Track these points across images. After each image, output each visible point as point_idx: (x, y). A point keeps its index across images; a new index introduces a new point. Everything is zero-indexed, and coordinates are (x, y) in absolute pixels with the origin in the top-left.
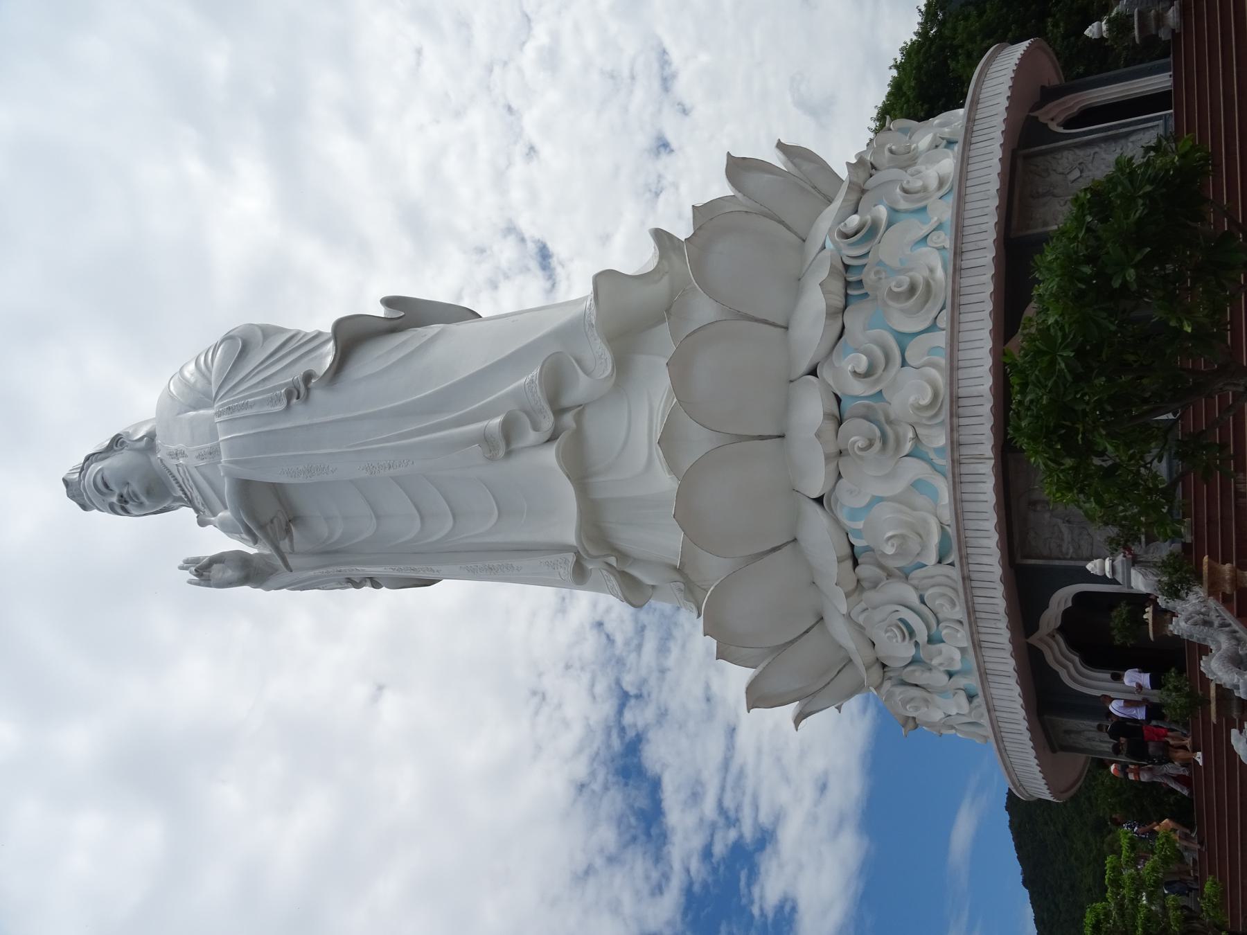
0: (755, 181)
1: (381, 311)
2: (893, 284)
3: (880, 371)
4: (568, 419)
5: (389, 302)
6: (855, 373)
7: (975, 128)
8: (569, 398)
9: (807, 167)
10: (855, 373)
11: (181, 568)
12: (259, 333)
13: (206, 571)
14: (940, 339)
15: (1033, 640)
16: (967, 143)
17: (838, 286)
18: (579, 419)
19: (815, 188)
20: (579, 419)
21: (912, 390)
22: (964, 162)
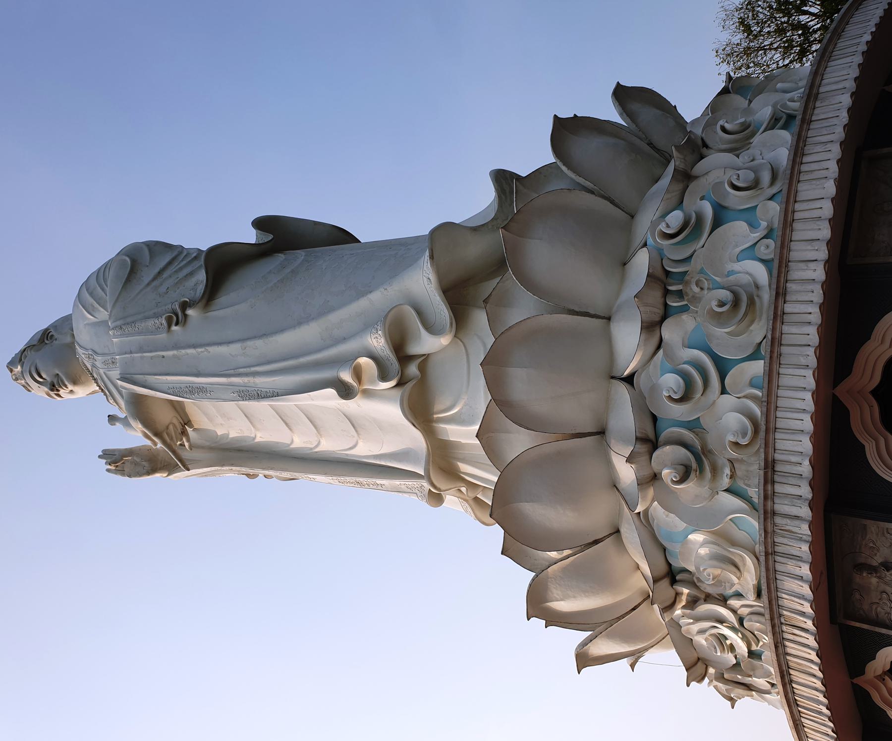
0: (587, 148)
1: (250, 236)
2: (714, 304)
3: (698, 395)
4: (413, 369)
5: (261, 224)
6: (670, 398)
7: (814, 118)
8: (415, 349)
9: (647, 114)
10: (670, 398)
11: (100, 457)
12: (146, 251)
13: (120, 461)
14: (758, 367)
15: (841, 391)
16: (807, 121)
17: (656, 295)
18: (422, 368)
19: (650, 144)
20: (422, 368)
21: (727, 416)
22: (798, 152)
